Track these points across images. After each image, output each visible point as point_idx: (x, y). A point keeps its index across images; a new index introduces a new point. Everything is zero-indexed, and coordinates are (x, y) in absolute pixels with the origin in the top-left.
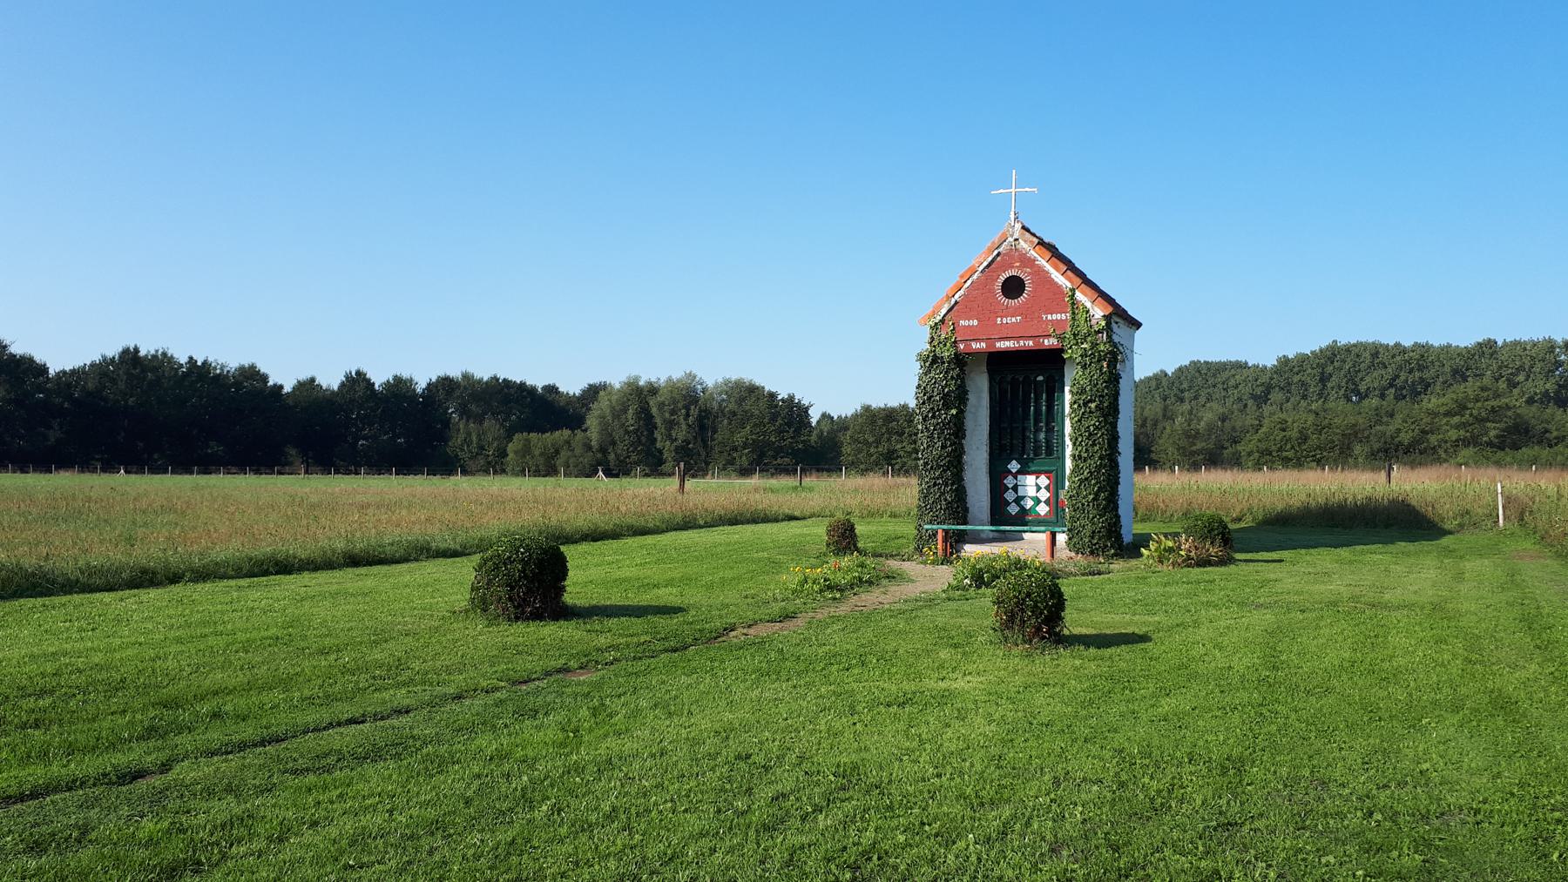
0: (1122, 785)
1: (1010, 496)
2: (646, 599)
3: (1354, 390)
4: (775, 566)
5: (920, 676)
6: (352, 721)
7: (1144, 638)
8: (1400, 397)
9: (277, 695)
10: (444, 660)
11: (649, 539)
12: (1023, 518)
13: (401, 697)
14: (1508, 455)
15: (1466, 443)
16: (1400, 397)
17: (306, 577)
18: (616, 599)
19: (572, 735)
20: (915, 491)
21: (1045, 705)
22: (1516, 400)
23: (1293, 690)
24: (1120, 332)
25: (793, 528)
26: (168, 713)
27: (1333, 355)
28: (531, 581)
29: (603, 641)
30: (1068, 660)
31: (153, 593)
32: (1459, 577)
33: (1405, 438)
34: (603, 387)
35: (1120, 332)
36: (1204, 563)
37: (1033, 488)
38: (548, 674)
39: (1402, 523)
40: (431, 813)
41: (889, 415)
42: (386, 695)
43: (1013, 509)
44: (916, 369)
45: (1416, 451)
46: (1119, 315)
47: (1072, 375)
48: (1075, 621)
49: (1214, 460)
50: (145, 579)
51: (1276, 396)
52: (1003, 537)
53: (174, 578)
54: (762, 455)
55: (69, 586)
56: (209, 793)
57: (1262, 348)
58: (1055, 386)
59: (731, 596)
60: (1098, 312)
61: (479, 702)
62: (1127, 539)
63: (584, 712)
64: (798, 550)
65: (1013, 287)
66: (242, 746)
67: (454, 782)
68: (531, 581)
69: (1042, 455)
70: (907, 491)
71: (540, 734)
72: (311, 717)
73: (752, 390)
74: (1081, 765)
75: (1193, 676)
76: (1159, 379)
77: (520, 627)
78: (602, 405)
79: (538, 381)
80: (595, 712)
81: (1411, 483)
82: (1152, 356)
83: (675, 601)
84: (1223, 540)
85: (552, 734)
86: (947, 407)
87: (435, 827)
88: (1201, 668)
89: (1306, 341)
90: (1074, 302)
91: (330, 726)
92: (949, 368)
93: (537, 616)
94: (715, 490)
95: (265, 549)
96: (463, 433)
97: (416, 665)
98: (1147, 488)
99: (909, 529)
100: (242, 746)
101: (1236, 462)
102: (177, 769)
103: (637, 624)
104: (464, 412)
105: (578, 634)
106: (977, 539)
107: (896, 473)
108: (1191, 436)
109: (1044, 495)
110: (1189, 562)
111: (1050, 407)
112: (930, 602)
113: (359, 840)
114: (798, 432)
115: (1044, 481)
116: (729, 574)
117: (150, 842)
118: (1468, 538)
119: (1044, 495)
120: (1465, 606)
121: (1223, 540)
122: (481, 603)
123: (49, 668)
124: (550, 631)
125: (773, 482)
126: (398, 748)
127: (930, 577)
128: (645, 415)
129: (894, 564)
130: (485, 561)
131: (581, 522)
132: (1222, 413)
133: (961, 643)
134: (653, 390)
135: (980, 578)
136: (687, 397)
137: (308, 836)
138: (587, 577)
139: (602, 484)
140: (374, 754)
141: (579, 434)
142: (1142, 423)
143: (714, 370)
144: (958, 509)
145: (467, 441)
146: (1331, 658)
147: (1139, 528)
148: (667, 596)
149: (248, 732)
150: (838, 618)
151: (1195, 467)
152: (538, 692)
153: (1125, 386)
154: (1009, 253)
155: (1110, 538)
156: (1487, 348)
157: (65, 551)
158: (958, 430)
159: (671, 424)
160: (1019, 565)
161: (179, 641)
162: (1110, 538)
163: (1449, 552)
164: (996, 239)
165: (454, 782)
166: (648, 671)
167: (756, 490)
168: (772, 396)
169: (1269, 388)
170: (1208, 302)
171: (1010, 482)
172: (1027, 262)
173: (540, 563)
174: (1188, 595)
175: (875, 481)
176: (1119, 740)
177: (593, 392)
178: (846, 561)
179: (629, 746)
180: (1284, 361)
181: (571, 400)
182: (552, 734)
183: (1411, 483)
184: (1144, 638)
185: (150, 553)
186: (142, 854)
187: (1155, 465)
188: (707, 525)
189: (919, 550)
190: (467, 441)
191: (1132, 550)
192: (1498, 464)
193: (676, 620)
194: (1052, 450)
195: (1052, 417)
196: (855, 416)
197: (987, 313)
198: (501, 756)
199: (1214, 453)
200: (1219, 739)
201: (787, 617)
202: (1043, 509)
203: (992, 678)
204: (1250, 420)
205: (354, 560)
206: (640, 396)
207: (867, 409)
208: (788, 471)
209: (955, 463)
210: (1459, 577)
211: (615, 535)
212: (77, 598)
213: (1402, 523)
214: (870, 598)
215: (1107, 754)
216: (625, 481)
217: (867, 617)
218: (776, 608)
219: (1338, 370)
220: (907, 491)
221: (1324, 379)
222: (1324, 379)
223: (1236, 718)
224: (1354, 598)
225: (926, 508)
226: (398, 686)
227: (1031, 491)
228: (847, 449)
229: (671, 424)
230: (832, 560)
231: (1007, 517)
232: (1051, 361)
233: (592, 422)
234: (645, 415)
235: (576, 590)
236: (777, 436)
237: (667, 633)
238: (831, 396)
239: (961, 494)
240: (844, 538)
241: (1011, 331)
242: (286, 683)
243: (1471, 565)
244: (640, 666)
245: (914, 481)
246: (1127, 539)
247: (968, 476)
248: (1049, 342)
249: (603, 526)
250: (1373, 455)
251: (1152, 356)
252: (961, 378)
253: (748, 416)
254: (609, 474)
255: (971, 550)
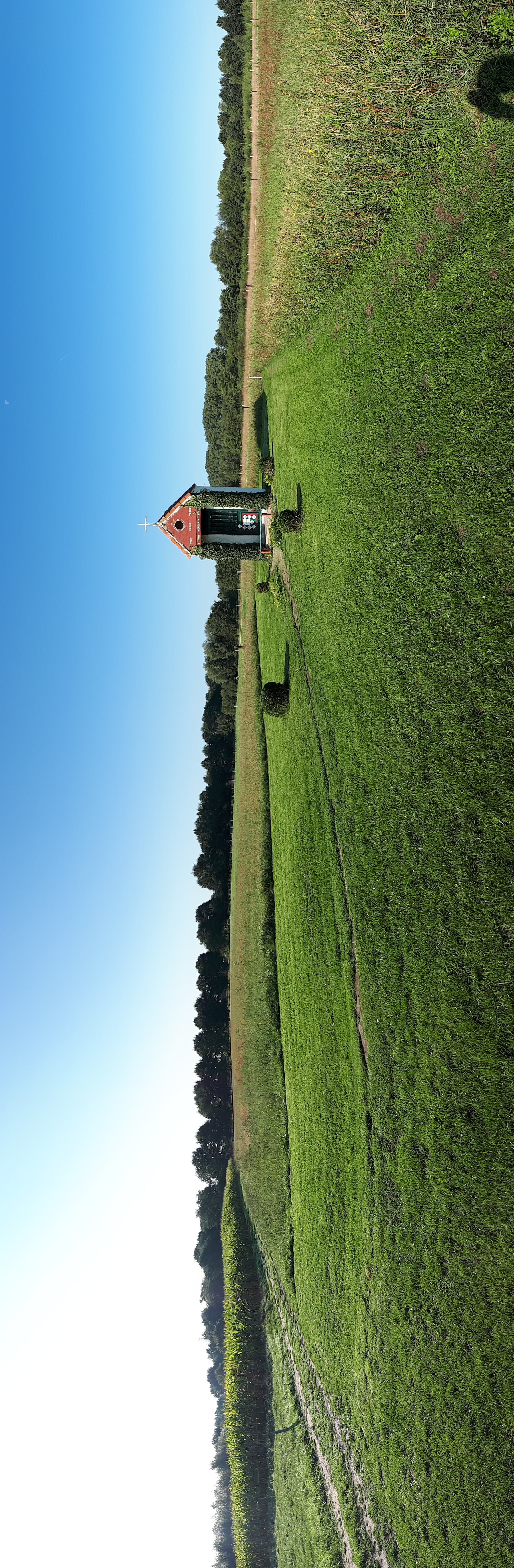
0: (350, 493)
1: (250, 528)
2: (283, 656)
3: (218, 416)
4: (272, 612)
5: (313, 558)
6: (320, 749)
7: (299, 486)
8: (221, 403)
9: (310, 775)
10: (300, 722)
11: (261, 657)
12: (257, 524)
13: (313, 736)
14: (240, 373)
15: (235, 385)
16: (221, 403)
17: (270, 772)
18: (283, 667)
19: (330, 676)
20: (247, 561)
21: (322, 516)
22: (223, 370)
23: (315, 441)
24: (196, 491)
25: (259, 605)
26: (313, 803)
27: (206, 423)
28: (275, 695)
29: (297, 669)
30: (306, 509)
31: (272, 815)
32: (278, 390)
33: (233, 402)
34: (207, 677)
35: (196, 491)
36: (273, 466)
37: (247, 520)
38: (308, 687)
39: (261, 405)
40: (354, 719)
41: (219, 572)
42: (312, 740)
43: (254, 527)
44: (206, 560)
45: (238, 399)
46: (191, 491)
47: (210, 506)
48: (293, 507)
49: (238, 463)
50: (268, 818)
51: (218, 442)
52: (264, 530)
53: (268, 810)
54: (231, 620)
55: (269, 838)
56: (341, 787)
57: (203, 446)
58: (213, 512)
59: (283, 626)
60: (189, 497)
61: (316, 710)
62: (264, 490)
63: (322, 673)
64: (266, 604)
65: (179, 525)
66: (326, 780)
67: (343, 714)
68: (275, 695)
69: (236, 518)
70: (246, 564)
71: (329, 687)
72: (318, 762)
73: (209, 623)
74: (343, 505)
75: (311, 470)
76: (210, 479)
77: (291, 699)
78: (213, 677)
79: (204, 702)
80: (323, 669)
81: (248, 401)
82: (203, 481)
83: (284, 645)
84: (266, 460)
85: (329, 683)
86: (219, 549)
87: (359, 717)
88: (309, 468)
89: (200, 432)
90: (186, 505)
91: (322, 755)
92: (206, 548)
93: (287, 693)
94: (244, 637)
95: (261, 785)
96: (221, 730)
97: (302, 732)
98: (247, 481)
99: (260, 563)
100: (326, 780)
101: (239, 456)
102: (332, 798)
103: (292, 658)
104: (214, 730)
105: (294, 678)
106: (264, 539)
107: (239, 569)
108: (230, 469)
109: (249, 517)
110: (273, 471)
111: (220, 514)
112: (286, 556)
113: (362, 740)
114: (224, 606)
115: (245, 517)
116: (275, 628)
117: (355, 800)
118: (265, 387)
119: (249, 517)
120: (287, 389)
121: (266, 460)
122: (282, 714)
123: (295, 838)
124: (293, 688)
125: (241, 616)
126: (330, 732)
127: (278, 556)
128: (216, 662)
129: (272, 569)
130: (268, 712)
131: (254, 681)
132: (223, 458)
133: (301, 544)
134: (208, 659)
135: (278, 538)
136: (211, 647)
137: (359, 756)
138: (273, 675)
139: (240, 678)
140: (333, 742)
141: (223, 686)
142: (225, 485)
143: (202, 637)
144: (254, 546)
145: (224, 728)
146: (305, 428)
147: (261, 486)
148: (282, 649)
149: (321, 780)
150: (292, 587)
151: (240, 468)
152: (314, 689)
153: (215, 489)
154: (168, 527)
155: (265, 495)
156: (207, 378)
157: (257, 870)
158: (227, 546)
159: (220, 653)
160: (274, 525)
161: (289, 805)
162: (265, 495)
163: (270, 392)
164: (162, 531)
165: (343, 714)
166: (309, 653)
167: (244, 620)
168: (211, 615)
169: (215, 444)
170: (187, 462)
171: (245, 528)
172: (171, 521)
173: (270, 691)
174: (284, 472)
175: (242, 576)
176: (334, 494)
177: (208, 681)
178: (271, 586)
179: (336, 656)
180: (207, 439)
181: (211, 689)
182: (329, 683)
183: (248, 401)
184: (299, 486)
185: (260, 818)
186: (359, 801)
187: (239, 481)
188: (257, 637)
189: (267, 560)
190: (224, 728)
191: (268, 488)
192: (242, 376)
193: (291, 644)
194: (235, 514)
195: (223, 513)
196: (219, 585)
197: (188, 535)
198: (336, 699)
199: (236, 463)
200: (333, 463)
201: (291, 605)
202: (254, 517)
203: (313, 534)
204: (225, 451)
205: (265, 758)
206: (210, 664)
207: (216, 580)
208: (237, 609)
209: (239, 547)
210: (278, 390)
211: (259, 670)
212: (273, 836)
213: (261, 405)
214: (285, 576)
215: (339, 498)
216: (239, 670)
217: (291, 576)
218: (288, 609)
219: (211, 421)
220: (246, 564)
221: (214, 427)
222: (214, 427)
223: (325, 458)
224: (285, 420)
225: (253, 557)
226: (309, 737)
227: (248, 521)
228: (230, 588)
229: (220, 653)
230: (271, 590)
231: (257, 529)
232: (205, 513)
233: (219, 681)
234: (216, 662)
235: (278, 678)
236: (225, 613)
237: (296, 647)
238: (211, 594)
239: (249, 545)
240: (263, 587)
241: (194, 526)
242: (306, 771)
243: (274, 386)
244: (307, 655)
245: (242, 562)
246: (264, 490)
247: (243, 543)
248: (199, 513)
249: (256, 674)
250: (238, 412)
251: (203, 481)
252: (209, 544)
253: (218, 624)
254: (237, 675)
255: (268, 542)
